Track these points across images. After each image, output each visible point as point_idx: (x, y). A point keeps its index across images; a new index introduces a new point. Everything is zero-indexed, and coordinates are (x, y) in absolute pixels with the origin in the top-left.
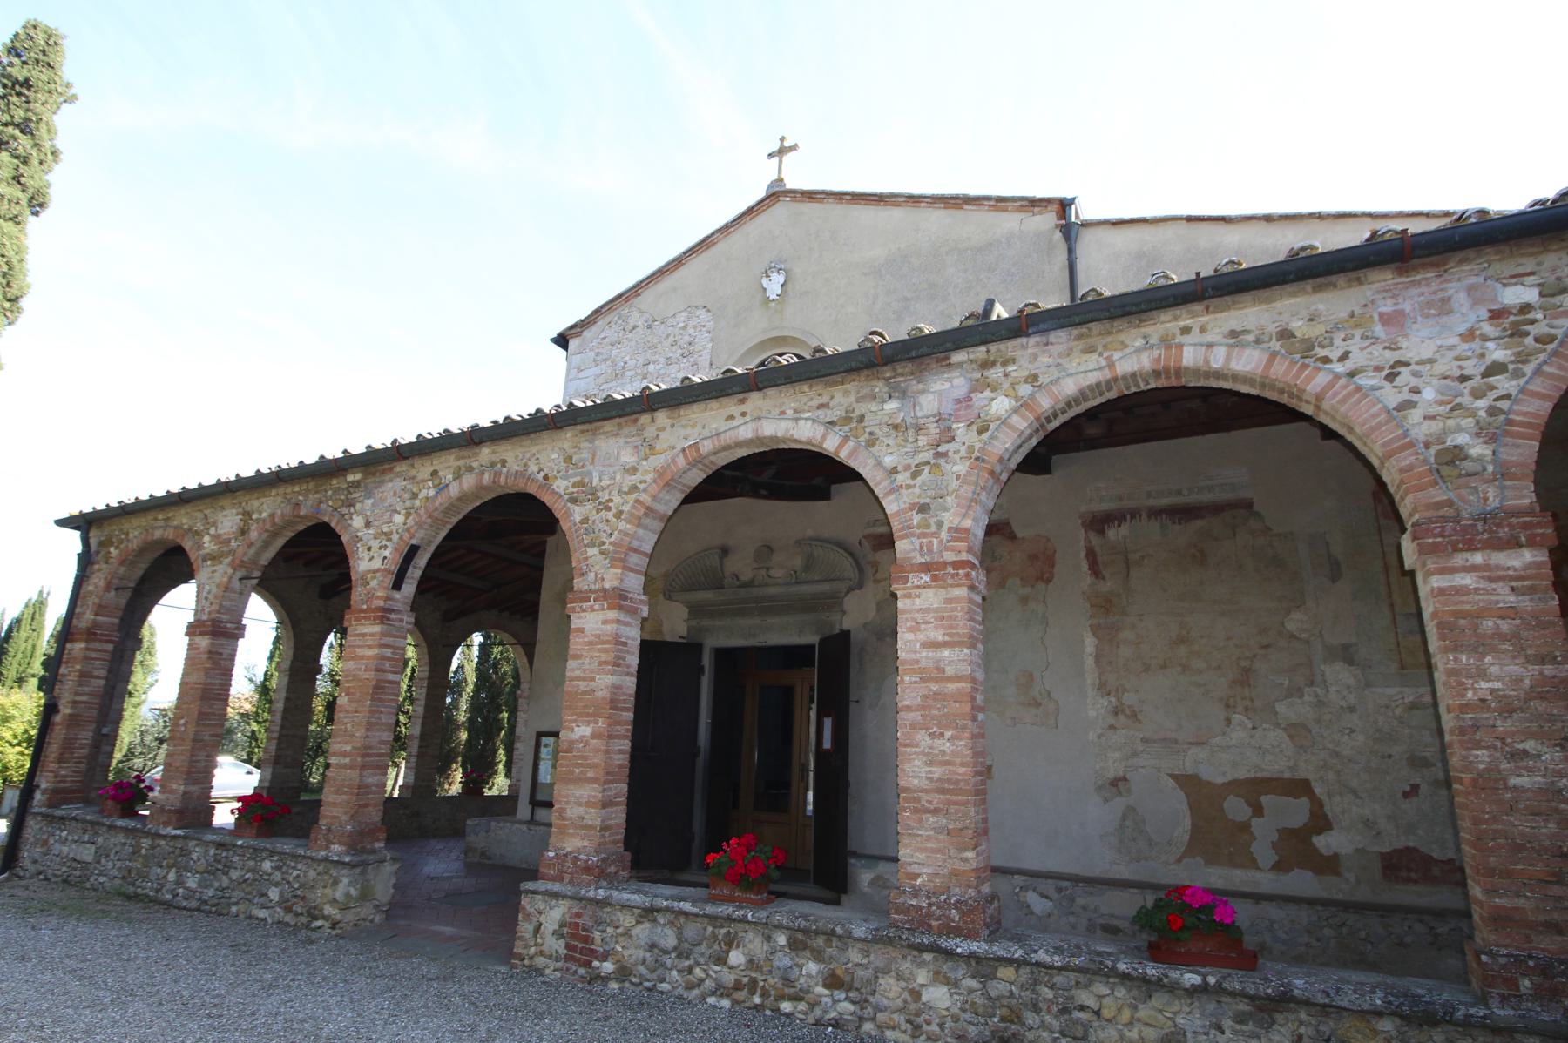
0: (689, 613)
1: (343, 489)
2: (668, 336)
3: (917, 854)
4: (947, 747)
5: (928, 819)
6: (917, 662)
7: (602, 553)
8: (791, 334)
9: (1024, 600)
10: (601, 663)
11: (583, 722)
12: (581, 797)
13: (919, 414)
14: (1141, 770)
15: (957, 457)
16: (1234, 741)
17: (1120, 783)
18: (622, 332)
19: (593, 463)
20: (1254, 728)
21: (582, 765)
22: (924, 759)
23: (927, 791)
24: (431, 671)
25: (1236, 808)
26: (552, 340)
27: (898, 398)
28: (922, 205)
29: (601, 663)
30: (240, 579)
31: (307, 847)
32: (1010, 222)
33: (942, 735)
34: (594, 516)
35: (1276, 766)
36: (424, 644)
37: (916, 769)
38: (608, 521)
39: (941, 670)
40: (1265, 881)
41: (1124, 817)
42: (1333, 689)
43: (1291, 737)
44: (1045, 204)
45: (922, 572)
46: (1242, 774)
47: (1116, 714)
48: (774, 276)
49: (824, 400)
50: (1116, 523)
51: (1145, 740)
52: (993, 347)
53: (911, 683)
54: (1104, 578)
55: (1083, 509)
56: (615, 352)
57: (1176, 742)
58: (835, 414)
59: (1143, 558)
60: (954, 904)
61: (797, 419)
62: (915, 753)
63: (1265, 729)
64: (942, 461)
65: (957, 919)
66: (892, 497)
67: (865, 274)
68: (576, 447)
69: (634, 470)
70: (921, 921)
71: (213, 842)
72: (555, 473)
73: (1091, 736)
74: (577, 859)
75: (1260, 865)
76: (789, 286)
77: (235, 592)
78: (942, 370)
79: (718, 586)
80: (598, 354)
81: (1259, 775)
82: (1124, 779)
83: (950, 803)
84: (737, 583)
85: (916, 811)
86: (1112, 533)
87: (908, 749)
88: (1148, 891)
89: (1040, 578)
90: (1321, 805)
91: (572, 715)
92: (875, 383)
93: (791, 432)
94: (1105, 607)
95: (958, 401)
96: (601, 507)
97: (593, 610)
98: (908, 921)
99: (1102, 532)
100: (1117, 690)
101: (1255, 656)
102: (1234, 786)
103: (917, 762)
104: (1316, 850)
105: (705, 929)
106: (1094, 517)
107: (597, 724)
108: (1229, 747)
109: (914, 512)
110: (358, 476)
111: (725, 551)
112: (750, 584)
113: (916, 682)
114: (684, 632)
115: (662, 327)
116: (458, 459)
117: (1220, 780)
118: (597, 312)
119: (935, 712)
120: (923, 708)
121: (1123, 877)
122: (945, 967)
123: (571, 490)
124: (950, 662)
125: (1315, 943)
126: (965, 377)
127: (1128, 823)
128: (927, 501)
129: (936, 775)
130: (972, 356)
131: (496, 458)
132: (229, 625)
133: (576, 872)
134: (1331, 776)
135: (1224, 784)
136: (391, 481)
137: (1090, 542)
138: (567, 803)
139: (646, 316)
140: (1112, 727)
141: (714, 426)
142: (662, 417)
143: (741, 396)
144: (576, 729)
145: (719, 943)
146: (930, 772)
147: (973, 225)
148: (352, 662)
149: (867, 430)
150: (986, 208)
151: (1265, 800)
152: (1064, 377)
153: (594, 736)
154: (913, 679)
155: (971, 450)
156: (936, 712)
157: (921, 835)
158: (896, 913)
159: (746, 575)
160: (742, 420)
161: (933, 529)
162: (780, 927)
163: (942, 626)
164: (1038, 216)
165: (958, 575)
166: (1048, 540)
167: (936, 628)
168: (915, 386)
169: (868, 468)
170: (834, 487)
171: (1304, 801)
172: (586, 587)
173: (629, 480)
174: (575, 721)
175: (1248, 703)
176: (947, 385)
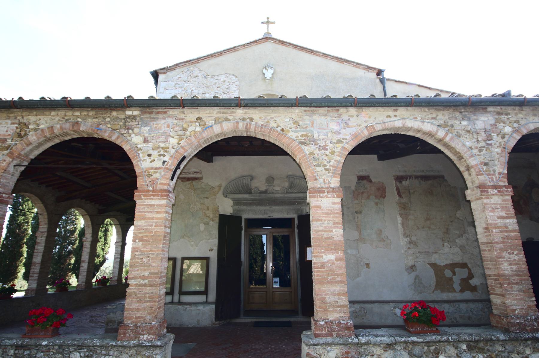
0: (233, 203)
1: (121, 119)
2: (216, 83)
3: (513, 301)
4: (516, 257)
5: (515, 287)
6: (497, 224)
7: (326, 170)
8: (276, 94)
9: (377, 204)
10: (334, 224)
11: (329, 253)
12: (335, 291)
13: (477, 128)
14: (419, 262)
15: (496, 146)
16: (445, 252)
17: (413, 268)
18: (190, 77)
19: (313, 126)
20: (451, 247)
21: (332, 275)
22: (508, 263)
23: (512, 276)
24: (48, 228)
25: (448, 273)
26: (150, 72)
27: (467, 120)
28: (328, 58)
29: (334, 224)
30: (15, 166)
31: (116, 339)
32: (361, 72)
33: (513, 253)
34: (317, 152)
35: (458, 259)
36: (46, 213)
37: (506, 267)
38: (327, 155)
39: (507, 227)
40: (458, 296)
41: (415, 279)
42: (470, 235)
43: (461, 250)
44: (373, 69)
45: (494, 189)
46: (449, 262)
47: (410, 243)
48: (269, 70)
49: (434, 116)
50: (405, 180)
51: (419, 252)
52: (503, 108)
53: (496, 233)
54: (402, 198)
55: (394, 174)
56: (186, 85)
57: (429, 252)
58: (441, 122)
59: (414, 192)
60: (534, 320)
61: (423, 122)
62: (504, 261)
63: (454, 248)
64: (490, 147)
65: (536, 325)
66: (472, 159)
67: (307, 78)
68: (300, 118)
69: (339, 133)
70: (522, 328)
71: (12, 346)
72: (288, 129)
73: (403, 251)
74: (339, 323)
75: (456, 291)
76: (275, 75)
77: (10, 174)
78: (484, 112)
79: (249, 191)
80: (176, 84)
81: (453, 262)
82: (414, 266)
83: (521, 280)
84: (259, 192)
85: (509, 284)
86: (404, 183)
87: (501, 259)
88: (435, 303)
89: (381, 196)
90: (471, 271)
91: (322, 249)
92: (455, 113)
93: (421, 127)
94: (404, 207)
95: (491, 125)
96: (321, 148)
97: (327, 197)
98: (517, 329)
99: (401, 182)
100: (410, 236)
101: (449, 225)
102: (446, 266)
103: (505, 264)
104: (470, 284)
105: (423, 348)
106: (398, 177)
107: (338, 253)
108: (444, 254)
109: (483, 165)
110: (136, 113)
111: (252, 178)
112: (265, 192)
113: (498, 232)
114: (232, 212)
115: (212, 79)
116: (219, 113)
117: (442, 264)
118: (177, 65)
119: (508, 244)
120: (503, 242)
121: (417, 300)
122: (536, 345)
123: (300, 138)
124: (510, 224)
125: (483, 314)
126: (493, 117)
127: (417, 281)
128: (488, 161)
129: (514, 269)
130: (496, 110)
131: (246, 116)
132: (4, 195)
133: (340, 330)
134: (472, 261)
135: (444, 265)
136: (164, 119)
137: (397, 185)
138: (326, 295)
139: (203, 73)
140: (409, 248)
141: (381, 119)
142: (352, 111)
143: (395, 108)
144: (325, 257)
145: (433, 354)
146: (511, 268)
147: (347, 69)
148: (143, 222)
149: (456, 131)
150: (353, 65)
151: (456, 270)
152: (529, 123)
153: (336, 259)
154: (497, 231)
155: (500, 143)
156: (509, 244)
157: (512, 294)
158: (512, 327)
159: (263, 188)
160: (395, 119)
161: (492, 172)
162: (462, 342)
163: (504, 210)
164: (370, 73)
165: (508, 191)
166: (383, 184)
167: (502, 211)
168: (473, 117)
169: (460, 146)
170: (214, 158)
171: (466, 270)
172: (319, 186)
173: (336, 138)
174: (324, 252)
175: (449, 239)
176: (486, 119)
